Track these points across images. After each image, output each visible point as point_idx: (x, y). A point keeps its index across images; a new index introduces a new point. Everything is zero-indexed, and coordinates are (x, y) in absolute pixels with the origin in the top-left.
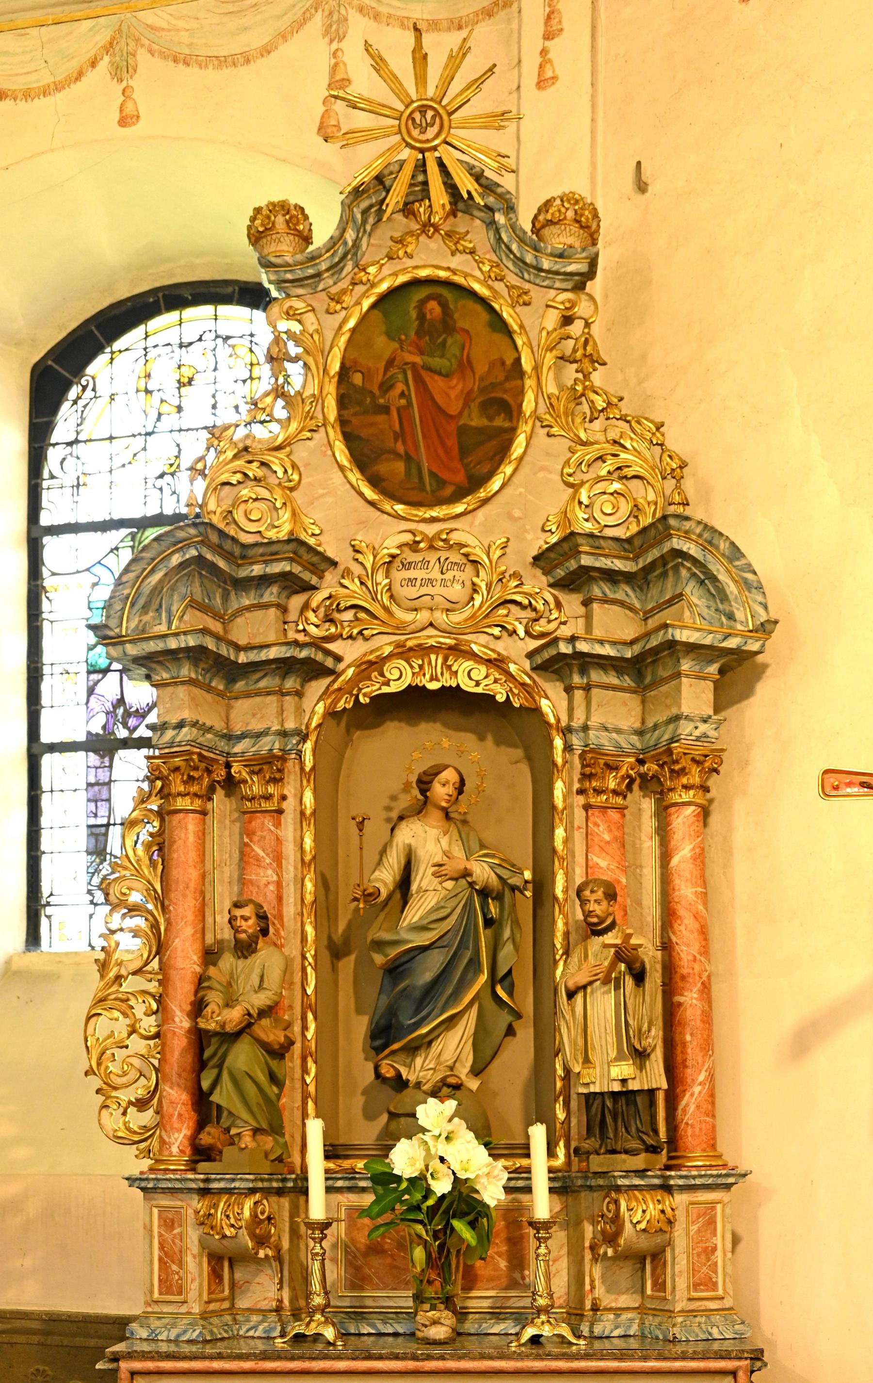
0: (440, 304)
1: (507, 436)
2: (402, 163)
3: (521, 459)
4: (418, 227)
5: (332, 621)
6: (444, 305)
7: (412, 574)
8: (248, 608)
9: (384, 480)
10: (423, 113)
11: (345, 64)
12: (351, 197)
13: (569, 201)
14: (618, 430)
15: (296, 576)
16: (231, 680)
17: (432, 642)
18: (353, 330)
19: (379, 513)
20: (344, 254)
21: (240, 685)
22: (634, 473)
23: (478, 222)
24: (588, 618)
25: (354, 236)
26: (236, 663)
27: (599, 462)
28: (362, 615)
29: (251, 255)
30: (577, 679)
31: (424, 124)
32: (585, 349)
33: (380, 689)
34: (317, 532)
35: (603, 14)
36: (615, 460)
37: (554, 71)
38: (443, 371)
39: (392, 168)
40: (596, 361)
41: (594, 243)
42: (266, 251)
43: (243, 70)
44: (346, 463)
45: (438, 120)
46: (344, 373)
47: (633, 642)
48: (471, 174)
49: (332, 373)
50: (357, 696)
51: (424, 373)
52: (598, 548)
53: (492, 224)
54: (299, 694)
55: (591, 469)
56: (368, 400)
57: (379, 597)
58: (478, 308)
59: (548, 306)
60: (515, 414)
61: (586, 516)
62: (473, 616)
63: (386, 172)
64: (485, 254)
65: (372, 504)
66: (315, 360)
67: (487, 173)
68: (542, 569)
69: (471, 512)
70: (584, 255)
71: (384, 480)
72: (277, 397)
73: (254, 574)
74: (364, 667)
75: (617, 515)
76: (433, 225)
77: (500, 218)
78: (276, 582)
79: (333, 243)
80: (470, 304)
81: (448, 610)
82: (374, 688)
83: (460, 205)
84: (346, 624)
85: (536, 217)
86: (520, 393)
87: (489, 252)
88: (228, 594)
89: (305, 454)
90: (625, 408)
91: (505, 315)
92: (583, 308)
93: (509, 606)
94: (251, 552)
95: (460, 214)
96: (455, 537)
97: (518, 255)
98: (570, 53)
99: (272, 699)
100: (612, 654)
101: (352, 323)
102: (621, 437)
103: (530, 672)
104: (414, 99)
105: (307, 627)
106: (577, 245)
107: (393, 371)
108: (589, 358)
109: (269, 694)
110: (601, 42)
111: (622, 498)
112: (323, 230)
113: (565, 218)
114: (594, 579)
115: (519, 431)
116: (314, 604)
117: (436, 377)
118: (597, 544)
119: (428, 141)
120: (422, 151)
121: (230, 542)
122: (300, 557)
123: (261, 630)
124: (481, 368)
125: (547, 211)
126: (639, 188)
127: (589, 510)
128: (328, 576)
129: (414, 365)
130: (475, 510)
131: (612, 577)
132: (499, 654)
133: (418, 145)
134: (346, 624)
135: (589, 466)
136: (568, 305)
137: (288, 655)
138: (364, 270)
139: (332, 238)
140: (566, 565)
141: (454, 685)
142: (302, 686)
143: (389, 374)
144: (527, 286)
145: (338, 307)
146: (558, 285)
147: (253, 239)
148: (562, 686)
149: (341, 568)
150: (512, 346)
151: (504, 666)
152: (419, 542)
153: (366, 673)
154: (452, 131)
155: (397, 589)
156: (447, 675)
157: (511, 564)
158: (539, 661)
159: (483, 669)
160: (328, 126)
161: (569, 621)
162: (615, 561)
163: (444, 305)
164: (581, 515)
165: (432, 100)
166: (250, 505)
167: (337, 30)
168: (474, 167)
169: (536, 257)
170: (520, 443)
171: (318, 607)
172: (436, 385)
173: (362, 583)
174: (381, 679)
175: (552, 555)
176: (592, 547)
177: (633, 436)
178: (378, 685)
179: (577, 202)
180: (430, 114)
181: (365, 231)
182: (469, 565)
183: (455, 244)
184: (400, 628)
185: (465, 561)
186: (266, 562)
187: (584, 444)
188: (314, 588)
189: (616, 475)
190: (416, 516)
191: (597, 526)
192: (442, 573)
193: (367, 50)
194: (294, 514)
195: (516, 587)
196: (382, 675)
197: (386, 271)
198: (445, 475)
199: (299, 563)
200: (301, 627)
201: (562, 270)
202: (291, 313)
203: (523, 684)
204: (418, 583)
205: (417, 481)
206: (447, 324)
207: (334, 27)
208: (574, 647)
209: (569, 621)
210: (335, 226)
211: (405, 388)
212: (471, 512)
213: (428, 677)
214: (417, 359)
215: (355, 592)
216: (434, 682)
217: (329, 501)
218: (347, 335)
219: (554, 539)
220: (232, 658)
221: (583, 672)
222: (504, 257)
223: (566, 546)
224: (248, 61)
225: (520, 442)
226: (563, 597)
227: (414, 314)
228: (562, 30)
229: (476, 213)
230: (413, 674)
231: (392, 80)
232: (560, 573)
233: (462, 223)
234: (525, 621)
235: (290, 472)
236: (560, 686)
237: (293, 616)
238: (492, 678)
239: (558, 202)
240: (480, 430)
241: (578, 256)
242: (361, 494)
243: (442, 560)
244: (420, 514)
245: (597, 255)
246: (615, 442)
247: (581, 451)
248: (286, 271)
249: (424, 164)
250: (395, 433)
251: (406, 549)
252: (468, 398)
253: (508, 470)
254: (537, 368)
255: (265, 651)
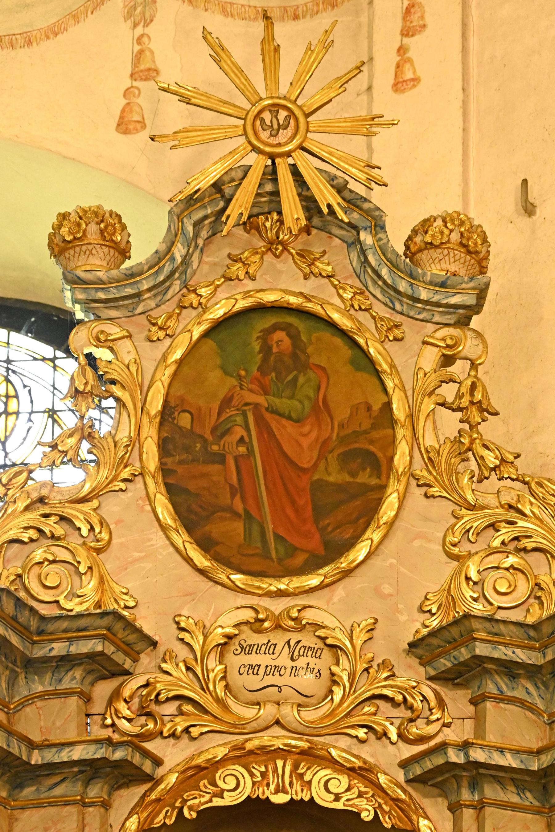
0: (288, 335)
1: (374, 496)
2: (247, 169)
3: (391, 524)
4: (262, 244)
5: (149, 714)
6: (294, 336)
7: (254, 659)
8: (42, 696)
9: (217, 543)
10: (275, 115)
11: (152, 52)
12: (182, 206)
13: (452, 221)
14: (514, 494)
15: (109, 658)
16: (17, 785)
17: (278, 743)
18: (180, 362)
19: (210, 584)
20: (171, 274)
21: (28, 792)
22: (534, 545)
23: (337, 241)
24: (479, 720)
25: (184, 252)
26: (28, 763)
27: (491, 531)
28: (188, 708)
29: (54, 271)
30: (466, 795)
31: (275, 126)
32: (472, 394)
33: (210, 801)
34: (132, 604)
35: (474, 11)
36: (512, 528)
37: (414, 72)
38: (293, 415)
39: (233, 174)
40: (486, 410)
41: (483, 270)
42: (72, 265)
43: (23, 53)
44: (170, 522)
45: (292, 122)
46: (167, 413)
47: (539, 752)
48: (332, 186)
49: (153, 412)
50: (181, 810)
51: (268, 416)
52: (496, 634)
53: (355, 243)
54: (106, 805)
55: (480, 539)
56: (199, 445)
57: (211, 688)
58: (338, 341)
59: (425, 343)
60: (384, 469)
61: (475, 595)
62: (332, 714)
63: (226, 179)
64: (346, 278)
65: (202, 572)
66: (132, 396)
67: (353, 185)
68: (420, 658)
69: (328, 585)
70: (472, 285)
71: (217, 543)
72: (82, 438)
73: (53, 654)
74: (190, 773)
75: (514, 595)
76: (281, 243)
77: (366, 238)
78: (80, 664)
79: (158, 259)
80: (327, 335)
81: (299, 705)
82: (203, 800)
83: (316, 221)
84: (166, 719)
85: (410, 238)
86: (392, 443)
87: (351, 276)
88: (17, 677)
89: (116, 509)
90: (523, 466)
91: (372, 351)
92: (469, 347)
93: (377, 702)
94: (51, 627)
95: (314, 231)
96: (309, 616)
97: (389, 282)
98: (434, 52)
99: (73, 810)
100: (514, 765)
101: (178, 354)
102: (519, 501)
103: (404, 785)
104: (263, 96)
105: (117, 721)
106: (462, 273)
107: (229, 412)
108: (476, 406)
109: (66, 804)
110: (474, 43)
111: (520, 575)
112: (144, 245)
113: (448, 241)
114: (487, 672)
115: (389, 490)
116: (126, 693)
117: (284, 421)
118: (495, 630)
119: (279, 145)
120: (272, 157)
121: (27, 613)
122: (115, 635)
123: (58, 724)
124: (342, 413)
125: (426, 232)
126: (526, 211)
127: (478, 588)
128: (144, 659)
129: (257, 406)
130: (333, 583)
131: (510, 670)
132: (365, 762)
133: (268, 149)
134: (166, 719)
135: (478, 534)
136: (449, 342)
137: (98, 756)
138: (195, 291)
139: (157, 252)
140: (454, 654)
141: (306, 799)
142: (110, 795)
143: (224, 417)
144: (398, 318)
145: (161, 334)
146: (437, 318)
147: (56, 250)
148: (446, 803)
149: (161, 649)
150: (380, 388)
151: (372, 776)
152: (263, 621)
153: (192, 780)
154: (309, 135)
155: (234, 678)
156: (297, 786)
157: (380, 650)
158: (419, 772)
159: (344, 780)
160: (130, 122)
161: (452, 722)
162: (516, 650)
163: (294, 336)
164: (468, 593)
165: (285, 98)
166: (46, 568)
167: (143, 13)
168: (336, 177)
169: (411, 285)
170: (392, 503)
171: (132, 697)
172: (285, 431)
173: (188, 669)
174: (212, 789)
175: (435, 641)
176: (489, 633)
177: (533, 500)
178: (208, 797)
179: (462, 223)
180: (283, 114)
181: (196, 246)
182: (326, 651)
183: (309, 266)
184: (238, 727)
185: (320, 645)
186: (70, 640)
187: (471, 508)
188: (127, 673)
189: (511, 547)
190: (259, 588)
191: (489, 607)
192: (292, 659)
193: (204, 38)
194: (101, 581)
195: (386, 679)
196: (214, 784)
197: (222, 294)
198: (295, 540)
199: (113, 643)
200: (109, 721)
201: (445, 301)
202: (102, 337)
203: (396, 800)
204: (262, 671)
205: (259, 545)
206: (298, 359)
207: (139, 9)
208: (467, 755)
209: (452, 722)
210: (161, 240)
211: (245, 434)
212: (328, 585)
213: (272, 787)
214: (261, 400)
215: (179, 679)
216: (281, 795)
217: (150, 569)
218: (173, 368)
219: (434, 623)
220: (24, 758)
221: (474, 786)
222: (370, 283)
223: (455, 631)
224: (29, 43)
225: (392, 500)
226: (446, 693)
227: (256, 346)
228: (424, 26)
229: (336, 231)
230: (254, 783)
231: (236, 74)
232: (445, 663)
233: (317, 242)
234: (397, 722)
235: (97, 530)
236: (442, 803)
237: (98, 707)
238: (355, 790)
239: (439, 222)
240: (340, 488)
241: (464, 286)
242: (189, 560)
243: (292, 643)
244: (264, 586)
245: (487, 285)
246: (510, 507)
247: (467, 516)
248: (97, 289)
249: (274, 172)
250: (231, 486)
251: (245, 628)
252: (324, 448)
253: (374, 535)
254: (412, 416)
255: (67, 750)
